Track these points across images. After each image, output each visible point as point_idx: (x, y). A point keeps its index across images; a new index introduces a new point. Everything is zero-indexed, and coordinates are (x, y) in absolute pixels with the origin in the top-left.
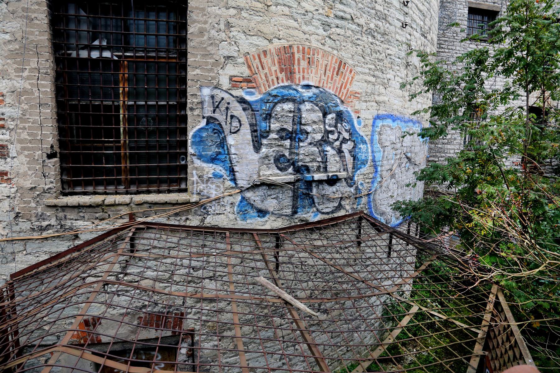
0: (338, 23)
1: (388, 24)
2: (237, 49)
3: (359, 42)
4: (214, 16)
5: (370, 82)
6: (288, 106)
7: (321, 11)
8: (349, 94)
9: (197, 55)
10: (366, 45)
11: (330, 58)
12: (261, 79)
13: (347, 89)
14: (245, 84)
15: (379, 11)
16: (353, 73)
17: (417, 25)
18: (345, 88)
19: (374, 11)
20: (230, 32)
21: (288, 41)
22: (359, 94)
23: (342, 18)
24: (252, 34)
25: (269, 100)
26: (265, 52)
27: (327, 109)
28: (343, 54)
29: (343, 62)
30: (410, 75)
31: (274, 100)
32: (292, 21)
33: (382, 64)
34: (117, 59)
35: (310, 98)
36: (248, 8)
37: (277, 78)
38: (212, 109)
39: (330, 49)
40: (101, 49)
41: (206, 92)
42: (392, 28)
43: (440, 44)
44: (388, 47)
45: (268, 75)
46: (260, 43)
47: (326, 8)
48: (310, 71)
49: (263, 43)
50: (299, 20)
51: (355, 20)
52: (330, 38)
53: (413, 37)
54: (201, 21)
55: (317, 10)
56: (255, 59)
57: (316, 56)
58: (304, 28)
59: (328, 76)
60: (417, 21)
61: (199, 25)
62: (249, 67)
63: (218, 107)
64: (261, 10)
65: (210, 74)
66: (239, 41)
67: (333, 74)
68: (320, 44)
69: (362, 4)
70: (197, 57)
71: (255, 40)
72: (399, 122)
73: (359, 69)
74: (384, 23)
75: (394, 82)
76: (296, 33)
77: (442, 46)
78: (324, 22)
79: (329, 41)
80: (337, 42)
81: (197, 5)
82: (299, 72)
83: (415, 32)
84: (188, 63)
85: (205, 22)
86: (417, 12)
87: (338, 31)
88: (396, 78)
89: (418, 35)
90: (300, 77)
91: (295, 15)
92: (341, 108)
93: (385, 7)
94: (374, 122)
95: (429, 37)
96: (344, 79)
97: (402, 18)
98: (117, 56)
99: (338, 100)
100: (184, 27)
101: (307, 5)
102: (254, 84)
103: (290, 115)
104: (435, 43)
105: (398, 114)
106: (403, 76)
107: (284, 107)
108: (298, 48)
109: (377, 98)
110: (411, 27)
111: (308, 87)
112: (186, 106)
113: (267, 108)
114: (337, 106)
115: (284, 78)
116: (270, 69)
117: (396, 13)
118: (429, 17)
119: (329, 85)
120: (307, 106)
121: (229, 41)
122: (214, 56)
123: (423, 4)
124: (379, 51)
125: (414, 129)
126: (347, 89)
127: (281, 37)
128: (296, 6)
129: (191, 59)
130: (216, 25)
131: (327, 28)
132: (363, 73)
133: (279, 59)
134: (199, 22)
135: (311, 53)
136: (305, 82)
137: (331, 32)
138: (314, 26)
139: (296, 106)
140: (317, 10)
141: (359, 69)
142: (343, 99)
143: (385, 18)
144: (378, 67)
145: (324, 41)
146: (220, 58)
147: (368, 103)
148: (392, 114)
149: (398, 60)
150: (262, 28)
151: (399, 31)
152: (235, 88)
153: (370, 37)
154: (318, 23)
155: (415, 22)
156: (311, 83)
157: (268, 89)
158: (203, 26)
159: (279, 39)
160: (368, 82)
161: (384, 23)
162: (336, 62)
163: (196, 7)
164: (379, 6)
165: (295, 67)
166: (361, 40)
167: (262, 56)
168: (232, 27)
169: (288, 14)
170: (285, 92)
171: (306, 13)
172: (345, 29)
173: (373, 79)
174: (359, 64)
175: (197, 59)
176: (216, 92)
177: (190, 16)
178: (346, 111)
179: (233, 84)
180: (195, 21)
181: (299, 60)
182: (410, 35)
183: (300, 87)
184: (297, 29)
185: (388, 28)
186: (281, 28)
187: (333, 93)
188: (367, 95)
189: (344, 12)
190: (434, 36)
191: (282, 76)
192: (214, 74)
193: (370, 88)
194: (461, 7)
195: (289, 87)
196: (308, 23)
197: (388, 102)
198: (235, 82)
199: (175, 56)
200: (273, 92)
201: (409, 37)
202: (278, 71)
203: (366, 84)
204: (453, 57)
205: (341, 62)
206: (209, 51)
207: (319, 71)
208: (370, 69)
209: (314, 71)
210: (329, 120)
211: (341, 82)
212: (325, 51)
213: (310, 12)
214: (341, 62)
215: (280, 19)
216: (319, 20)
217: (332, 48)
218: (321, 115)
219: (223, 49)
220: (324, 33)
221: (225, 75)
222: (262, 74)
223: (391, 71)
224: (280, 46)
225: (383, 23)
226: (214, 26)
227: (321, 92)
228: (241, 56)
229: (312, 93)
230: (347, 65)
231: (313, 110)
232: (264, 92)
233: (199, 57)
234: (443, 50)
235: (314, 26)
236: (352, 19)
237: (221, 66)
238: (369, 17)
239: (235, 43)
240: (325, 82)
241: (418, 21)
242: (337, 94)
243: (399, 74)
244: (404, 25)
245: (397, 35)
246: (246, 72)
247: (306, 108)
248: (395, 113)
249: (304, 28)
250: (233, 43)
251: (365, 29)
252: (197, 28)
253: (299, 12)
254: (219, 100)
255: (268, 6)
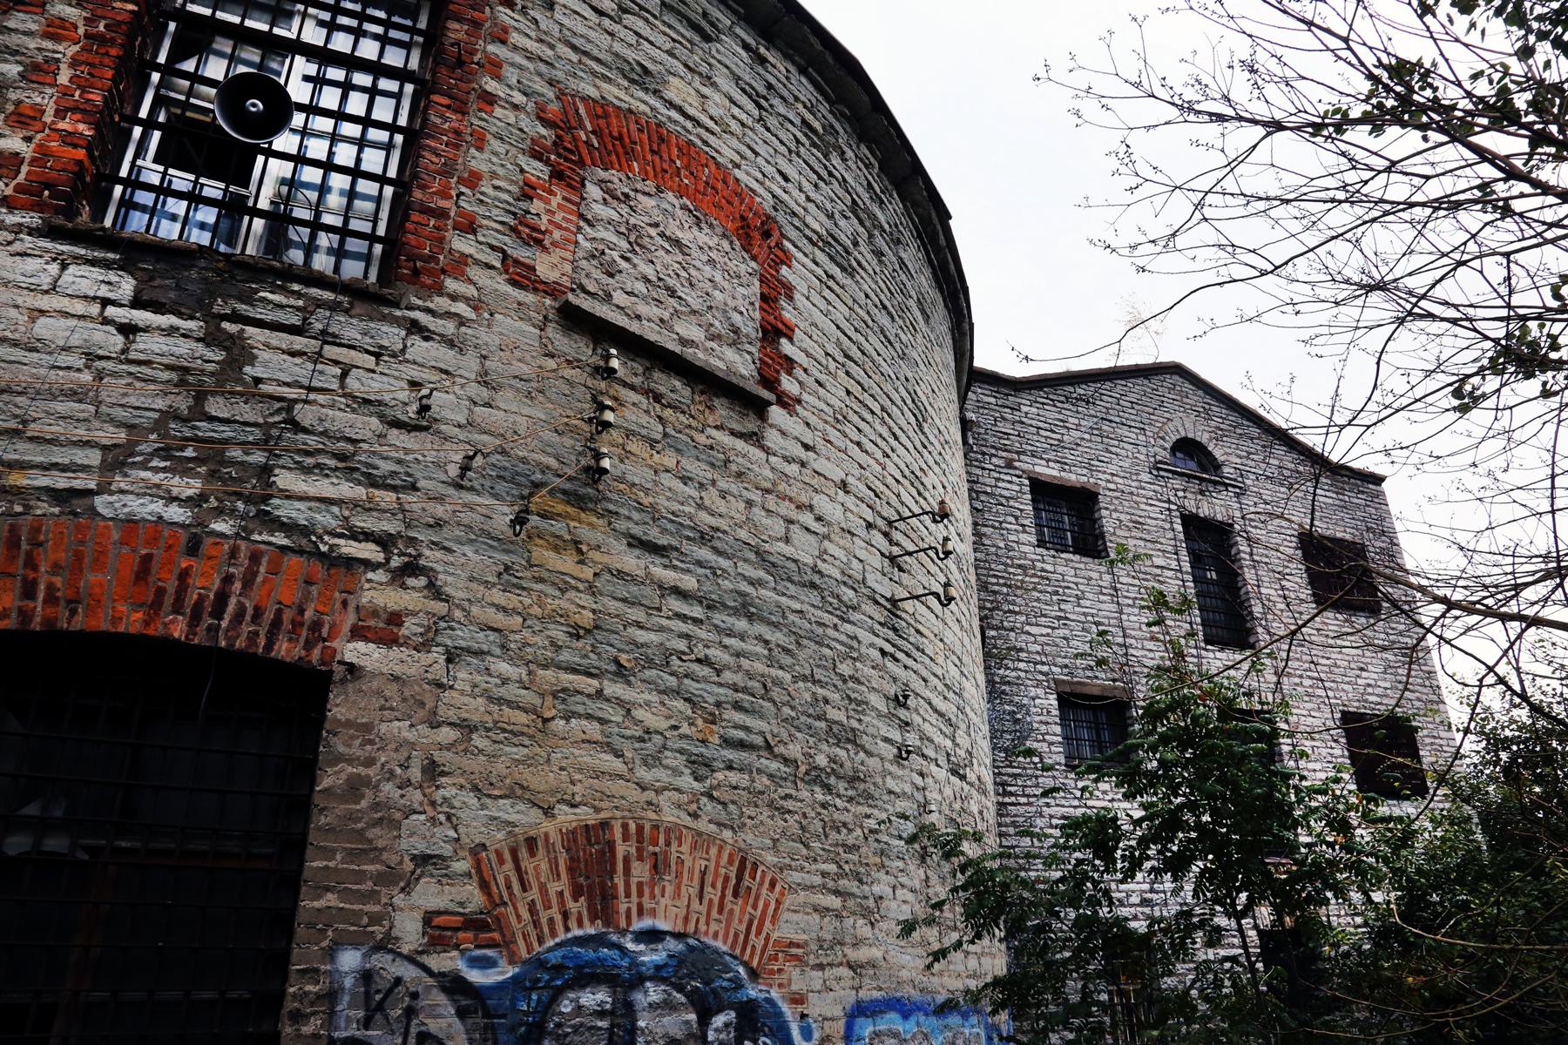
0: (731, 757)
1: (862, 754)
2: (452, 833)
3: (789, 804)
4: (393, 746)
5: (828, 909)
6: (597, 997)
7: (685, 729)
8: (770, 951)
9: (334, 851)
10: (808, 811)
11: (714, 851)
12: (517, 918)
13: (764, 935)
14: (470, 935)
15: (836, 722)
16: (778, 888)
17: (937, 748)
18: (758, 933)
19: (823, 724)
20: (438, 787)
21: (597, 810)
22: (798, 946)
23: (742, 745)
24: (496, 793)
25: (539, 980)
26: (531, 843)
27: (711, 999)
28: (749, 837)
29: (751, 859)
30: (934, 879)
31: (552, 979)
32: (610, 757)
33: (856, 858)
34: (86, 857)
35: (658, 968)
36: (490, 725)
37: (566, 915)
38: (361, 1014)
39: (713, 827)
40: (43, 826)
41: (350, 960)
42: (873, 763)
43: (1004, 784)
44: (868, 811)
45: (539, 906)
46: (519, 816)
47: (700, 722)
48: (657, 891)
49: (524, 817)
50: (629, 754)
51: (776, 749)
52: (711, 797)
53: (929, 780)
54: (358, 758)
55: (675, 728)
56: (501, 861)
57: (674, 847)
58: (642, 773)
59: (711, 901)
60: (936, 740)
61: (350, 770)
62: (484, 886)
63: (380, 1007)
64: (525, 730)
65: (367, 908)
66: (459, 813)
67: (723, 896)
68: (684, 816)
69: (793, 708)
70: (332, 858)
71: (507, 810)
72: (922, 1018)
73: (796, 877)
74: (852, 753)
75: (893, 905)
76: (618, 787)
77: (1009, 789)
78: (693, 758)
79: (708, 806)
80: (732, 807)
81: (351, 717)
82: (628, 895)
83: (933, 767)
84: (306, 874)
85: (370, 762)
86: (933, 718)
87: (734, 777)
88: (899, 892)
89: (942, 774)
90: (629, 910)
91: (617, 742)
92: (752, 992)
93: (852, 713)
94: (849, 1027)
95: (971, 777)
96: (755, 907)
97: (896, 735)
98: (86, 849)
99: (741, 970)
100: (308, 769)
101: (649, 715)
102: (496, 935)
103: (600, 1024)
104: (990, 787)
105: (915, 995)
106: (917, 884)
107: (583, 1001)
108: (625, 826)
109: (853, 955)
110: (923, 755)
111: (652, 936)
112: (281, 1006)
113: (533, 1004)
114: (738, 985)
115: (585, 913)
116: (543, 889)
117: (880, 725)
118: (963, 726)
119: (714, 927)
120: (654, 992)
121: (431, 812)
122: (385, 856)
123: (945, 698)
124: (845, 825)
125: (967, 1031)
126: (764, 935)
127: (578, 799)
128: (619, 719)
129: (314, 864)
130: (398, 771)
131: (703, 771)
132: (806, 888)
133: (572, 859)
134: (350, 761)
135: (661, 841)
136: (646, 923)
137: (715, 782)
138: (667, 767)
139: (620, 996)
140: (675, 728)
141: (796, 877)
142: (755, 964)
143: (851, 738)
144: (846, 867)
145: (694, 806)
146: (401, 862)
147: (828, 972)
148: (899, 995)
149: (897, 842)
150: (527, 776)
151: (894, 769)
152: (439, 948)
153: (817, 789)
154: (677, 761)
155: (932, 741)
156: (663, 925)
157: (537, 948)
158: (361, 770)
159: (573, 806)
160: (823, 911)
161: (852, 753)
162: (731, 862)
163: (348, 721)
164: (835, 711)
165: (616, 880)
166: (796, 799)
167: (523, 853)
168: (443, 774)
169: (599, 738)
170: (588, 954)
171: (646, 737)
172: (751, 772)
173: (835, 902)
174: (793, 863)
175: (331, 864)
176: (381, 961)
177: (328, 745)
178: (766, 1000)
179: (432, 937)
180: (339, 759)
181: (627, 860)
182: (922, 775)
183: (629, 936)
184: (621, 777)
185: (862, 763)
186: (577, 777)
187: (725, 948)
188: (821, 947)
189: (747, 729)
190: (982, 770)
191: (577, 907)
192: (377, 908)
193: (829, 926)
194: (1040, 692)
195: (598, 940)
196: (652, 761)
197: (883, 963)
198: (438, 931)
199: (270, 851)
200: (550, 955)
201: (919, 781)
202: (567, 895)
203: (816, 917)
204: (1041, 816)
205: (743, 861)
206: (370, 841)
207: (684, 889)
208: (824, 874)
209: (669, 889)
210: (716, 1030)
211: (747, 917)
212: (700, 834)
213: (657, 732)
214: (743, 861)
215: (577, 752)
216: (681, 751)
217: (719, 824)
218: (693, 1017)
219: (411, 835)
220: (695, 784)
221: (412, 908)
222: (519, 905)
223: (882, 875)
224: (574, 824)
225: (848, 751)
226: (391, 772)
227: (691, 949)
228: (462, 854)
229: (664, 954)
230: (761, 868)
231: (668, 1006)
232: (524, 954)
233: (339, 857)
234: (1013, 799)
235: (667, 767)
236: (769, 747)
237: (402, 884)
238: (812, 740)
239: (449, 818)
240: (703, 920)
241: (938, 739)
242: (738, 952)
243: (904, 880)
244: (903, 754)
245: (889, 780)
246: (472, 897)
247: (650, 999)
248: (909, 992)
249: (642, 773)
250: (442, 818)
251: (803, 769)
252: (343, 776)
253: (628, 733)
254: (386, 986)
255: (546, 721)
